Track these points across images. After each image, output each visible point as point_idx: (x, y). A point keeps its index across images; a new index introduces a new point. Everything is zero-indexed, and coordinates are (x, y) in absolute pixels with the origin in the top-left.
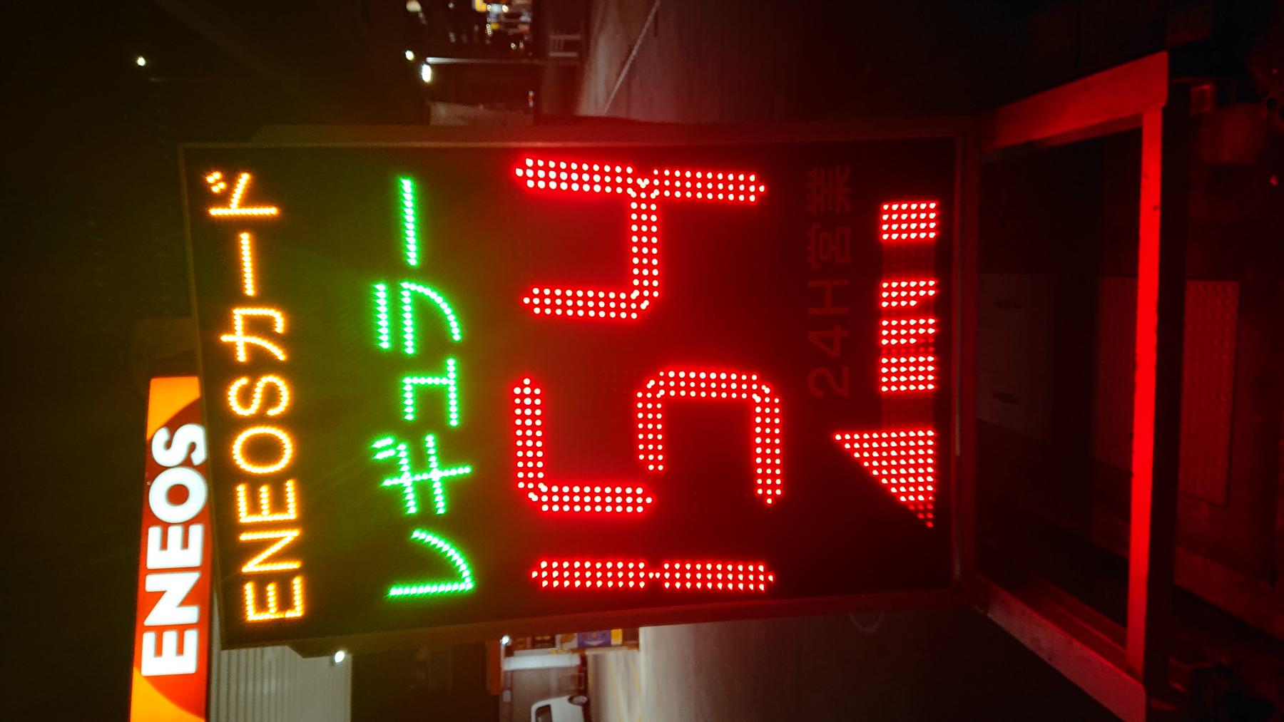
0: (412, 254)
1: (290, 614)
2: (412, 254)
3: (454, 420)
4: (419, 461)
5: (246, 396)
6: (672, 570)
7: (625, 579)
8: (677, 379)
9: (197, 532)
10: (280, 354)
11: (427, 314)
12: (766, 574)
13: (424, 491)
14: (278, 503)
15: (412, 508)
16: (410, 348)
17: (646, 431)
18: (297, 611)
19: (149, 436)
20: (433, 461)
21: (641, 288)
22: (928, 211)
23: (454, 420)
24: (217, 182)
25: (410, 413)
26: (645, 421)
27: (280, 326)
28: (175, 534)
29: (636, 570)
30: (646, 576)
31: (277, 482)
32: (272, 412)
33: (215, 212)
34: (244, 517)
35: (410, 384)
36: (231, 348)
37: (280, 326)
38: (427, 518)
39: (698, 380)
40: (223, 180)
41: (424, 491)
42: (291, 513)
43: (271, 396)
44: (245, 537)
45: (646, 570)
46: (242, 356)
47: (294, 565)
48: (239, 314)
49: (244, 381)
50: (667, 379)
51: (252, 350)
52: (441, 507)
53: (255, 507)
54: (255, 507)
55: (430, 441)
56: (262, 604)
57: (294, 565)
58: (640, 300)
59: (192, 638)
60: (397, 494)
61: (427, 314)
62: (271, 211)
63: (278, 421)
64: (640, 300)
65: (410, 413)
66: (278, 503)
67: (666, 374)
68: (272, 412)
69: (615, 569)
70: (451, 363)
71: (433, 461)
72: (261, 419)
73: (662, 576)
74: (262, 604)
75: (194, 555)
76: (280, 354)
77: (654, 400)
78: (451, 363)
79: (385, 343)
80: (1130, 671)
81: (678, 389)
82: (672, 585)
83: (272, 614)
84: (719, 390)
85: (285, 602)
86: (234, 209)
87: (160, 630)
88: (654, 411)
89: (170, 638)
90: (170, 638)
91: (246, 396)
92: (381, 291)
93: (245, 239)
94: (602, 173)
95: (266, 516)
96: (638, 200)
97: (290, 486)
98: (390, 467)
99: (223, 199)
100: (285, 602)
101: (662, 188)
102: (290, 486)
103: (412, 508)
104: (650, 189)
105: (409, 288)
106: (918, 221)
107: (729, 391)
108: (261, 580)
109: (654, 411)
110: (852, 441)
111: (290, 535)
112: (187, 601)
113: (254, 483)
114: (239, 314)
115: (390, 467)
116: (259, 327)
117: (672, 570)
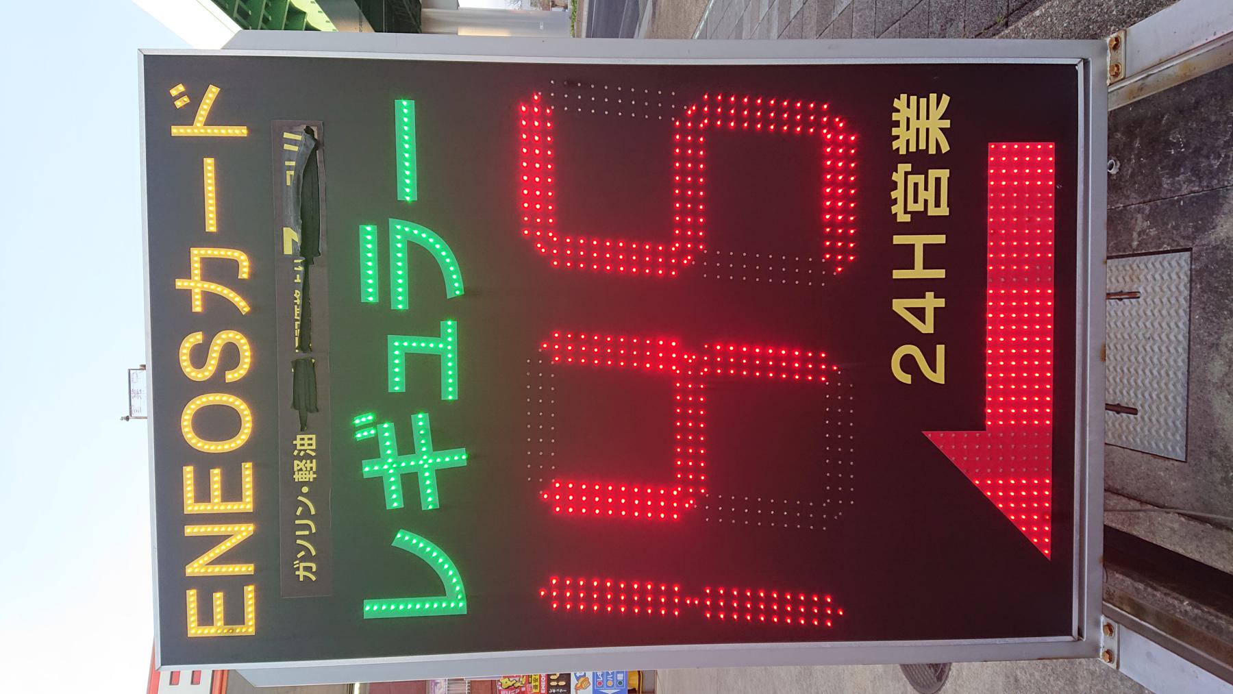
0: (408, 191)
1: (239, 630)
2: (408, 191)
3: (450, 392)
4: (406, 446)
5: (199, 357)
6: (715, 596)
10: (243, 305)
11: (420, 258)
12: (833, 606)
13: (410, 482)
14: (232, 491)
15: (395, 501)
16: (400, 302)
18: (249, 627)
20: (423, 443)
21: (683, 239)
22: (1045, 153)
23: (450, 392)
24: (181, 95)
25: (397, 382)
27: (244, 273)
29: (670, 594)
30: (682, 602)
31: (230, 463)
32: (232, 376)
33: (177, 131)
34: (191, 506)
35: (399, 347)
37: (244, 273)
38: (412, 517)
41: (410, 482)
42: (247, 504)
43: (230, 356)
44: (190, 530)
45: (681, 595)
46: (197, 306)
47: (247, 569)
48: (198, 254)
49: (197, 338)
51: (208, 297)
52: (430, 499)
53: (203, 494)
54: (203, 494)
55: (421, 421)
56: (206, 617)
57: (247, 569)
58: (682, 253)
60: (377, 483)
61: (419, 256)
62: (241, 131)
63: (234, 388)
64: (682, 253)
65: (397, 382)
66: (232, 491)
67: (712, 347)
68: (232, 376)
70: (450, 327)
71: (423, 443)
72: (216, 384)
73: (702, 603)
74: (206, 617)
76: (243, 305)
77: (696, 132)
78: (450, 327)
79: (357, 421)
82: (715, 616)
83: (218, 628)
85: (234, 615)
86: (199, 128)
91: (199, 357)
92: (369, 234)
93: (211, 226)
95: (217, 505)
97: (247, 470)
99: (187, 117)
100: (234, 615)
101: (712, 364)
102: (247, 470)
103: (395, 501)
104: (698, 365)
105: (403, 231)
106: (1020, 321)
108: (207, 586)
111: (244, 531)
113: (204, 463)
114: (198, 254)
115: (372, 449)
116: (219, 271)
117: (715, 596)
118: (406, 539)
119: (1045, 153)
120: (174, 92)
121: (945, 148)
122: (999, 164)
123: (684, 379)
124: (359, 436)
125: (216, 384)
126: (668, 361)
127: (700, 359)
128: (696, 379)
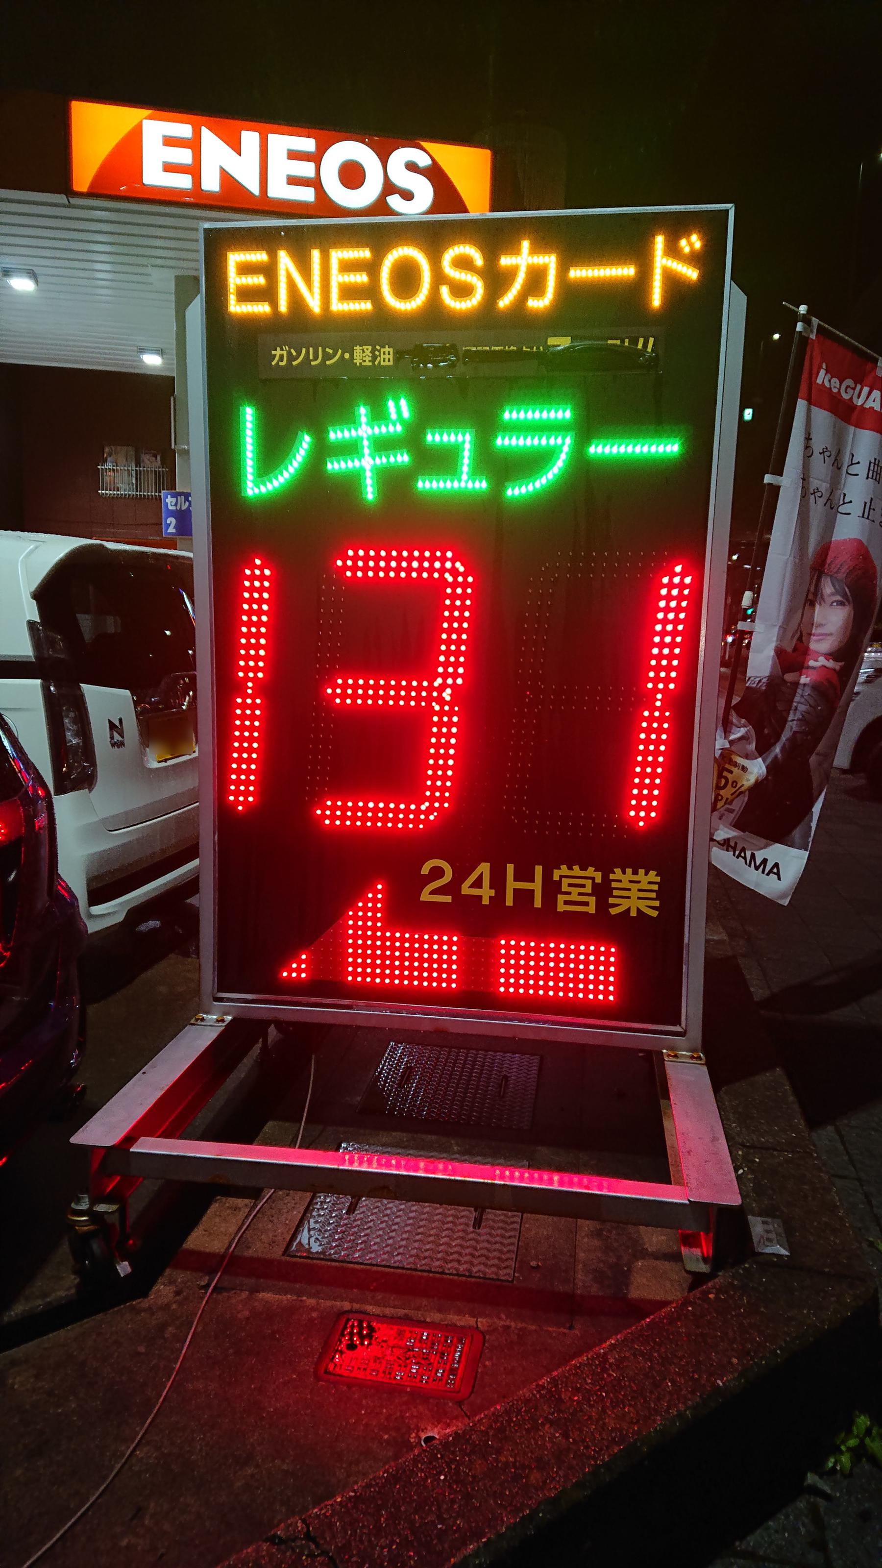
4: (383, 445)
5: (464, 263)
6: (253, 707)
7: (247, 657)
8: (450, 724)
9: (307, 195)
13: (350, 449)
14: (350, 293)
17: (398, 688)
19: (424, 144)
24: (691, 244)
25: (434, 438)
26: (409, 688)
27: (281, 364)
28: (306, 169)
29: (256, 669)
31: (371, 292)
34: (337, 255)
36: (516, 251)
37: (281, 364)
39: (448, 746)
40: (692, 251)
41: (350, 449)
43: (461, 291)
50: (450, 714)
52: (334, 466)
53: (348, 267)
54: (348, 267)
55: (403, 458)
56: (246, 269)
59: (184, 182)
65: (434, 438)
66: (350, 293)
69: (258, 646)
72: (439, 278)
74: (246, 269)
75: (279, 190)
76: (505, 302)
78: (482, 485)
80: (130, 1138)
81: (440, 724)
83: (234, 280)
84: (436, 767)
85: (246, 295)
87: (194, 144)
88: (418, 699)
89: (184, 156)
90: (184, 156)
92: (564, 413)
94: (671, 657)
95: (337, 279)
96: (430, 689)
98: (379, 414)
99: (672, 250)
100: (246, 295)
101: (441, 713)
103: (335, 435)
104: (441, 701)
107: (434, 778)
108: (269, 270)
109: (418, 699)
110: (375, 900)
111: (314, 304)
112: (226, 177)
113: (372, 268)
115: (379, 414)
117: (253, 707)
118: (305, 442)
119: (606, 993)
120: (694, 238)
121: (613, 911)
122: (597, 953)
123: (430, 689)
124: (391, 404)
125: (439, 278)
126: (445, 676)
127: (447, 703)
128: (429, 699)
